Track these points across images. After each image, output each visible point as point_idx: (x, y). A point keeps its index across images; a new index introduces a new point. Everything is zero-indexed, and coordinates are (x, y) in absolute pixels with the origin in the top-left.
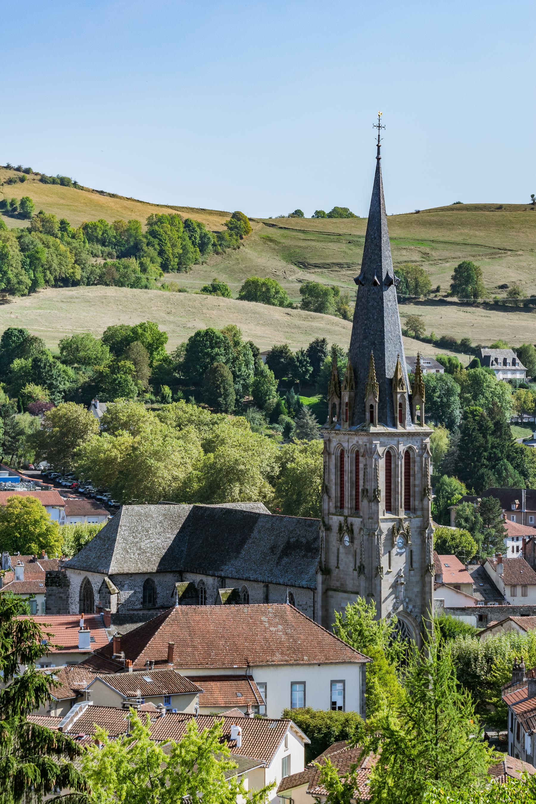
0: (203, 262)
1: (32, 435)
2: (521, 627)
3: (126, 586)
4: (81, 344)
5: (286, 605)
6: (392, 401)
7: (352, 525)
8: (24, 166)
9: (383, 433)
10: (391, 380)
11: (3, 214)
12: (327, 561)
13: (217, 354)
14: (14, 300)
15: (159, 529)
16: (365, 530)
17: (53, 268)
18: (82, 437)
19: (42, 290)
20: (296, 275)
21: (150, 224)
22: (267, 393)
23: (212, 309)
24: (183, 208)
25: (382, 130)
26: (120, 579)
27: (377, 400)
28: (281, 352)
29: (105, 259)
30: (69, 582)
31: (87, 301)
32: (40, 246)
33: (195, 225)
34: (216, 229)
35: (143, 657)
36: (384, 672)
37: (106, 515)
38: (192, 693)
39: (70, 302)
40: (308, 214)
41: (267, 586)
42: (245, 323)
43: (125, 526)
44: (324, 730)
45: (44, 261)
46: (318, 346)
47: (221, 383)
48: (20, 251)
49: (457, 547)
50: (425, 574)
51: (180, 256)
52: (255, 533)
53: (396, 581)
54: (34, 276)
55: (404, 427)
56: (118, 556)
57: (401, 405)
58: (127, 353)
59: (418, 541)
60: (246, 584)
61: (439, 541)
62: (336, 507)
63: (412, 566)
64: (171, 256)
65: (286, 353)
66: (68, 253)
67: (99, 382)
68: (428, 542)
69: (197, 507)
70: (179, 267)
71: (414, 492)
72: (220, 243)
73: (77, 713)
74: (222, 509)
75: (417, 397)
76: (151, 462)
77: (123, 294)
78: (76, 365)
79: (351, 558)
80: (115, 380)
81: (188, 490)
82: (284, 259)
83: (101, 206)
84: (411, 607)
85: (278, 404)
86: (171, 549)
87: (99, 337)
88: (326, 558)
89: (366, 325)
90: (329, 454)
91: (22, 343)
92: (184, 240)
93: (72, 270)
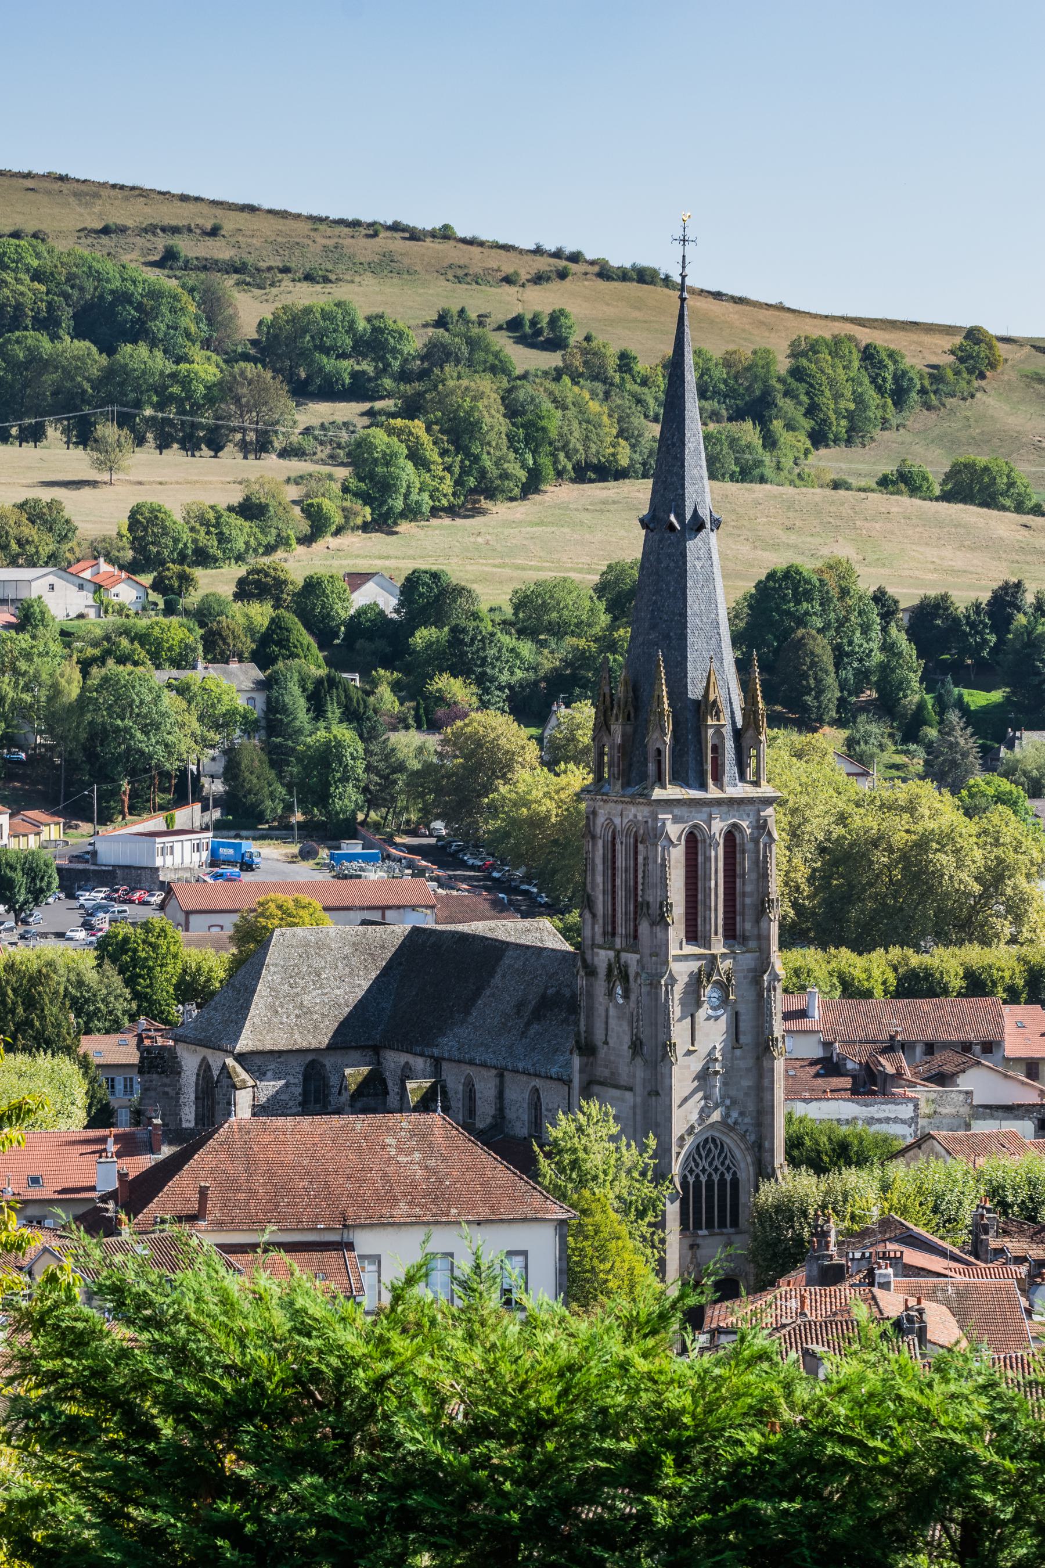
0: (898, 426)
3: (269, 1074)
4: (552, 597)
6: (700, 742)
7: (626, 966)
8: (569, 248)
9: (678, 801)
11: (516, 343)
13: (807, 613)
14: (494, 509)
16: (644, 975)
17: (571, 446)
18: (503, 776)
21: (793, 355)
22: (902, 685)
23: (874, 519)
24: (876, 320)
25: (689, 247)
26: (258, 1061)
27: (667, 739)
28: (937, 606)
30: (181, 1067)
32: (547, 405)
33: (884, 355)
34: (935, 360)
39: (601, 511)
41: (501, 1076)
42: (937, 546)
43: (276, 965)
45: (553, 434)
46: (1006, 594)
47: (810, 668)
48: (505, 416)
50: (764, 1055)
51: (850, 416)
52: (497, 980)
53: (706, 1069)
54: (535, 463)
55: (721, 788)
57: (715, 748)
59: (750, 995)
60: (470, 1070)
63: (737, 1040)
64: (833, 417)
65: (948, 608)
67: (580, 667)
68: (769, 997)
70: (850, 437)
71: (744, 905)
72: (934, 387)
75: (750, 733)
78: (542, 637)
83: (712, 322)
84: (735, 1114)
85: (921, 706)
86: (361, 1006)
88: (587, 1025)
89: (655, 602)
91: (437, 597)
92: (861, 384)
93: (612, 450)
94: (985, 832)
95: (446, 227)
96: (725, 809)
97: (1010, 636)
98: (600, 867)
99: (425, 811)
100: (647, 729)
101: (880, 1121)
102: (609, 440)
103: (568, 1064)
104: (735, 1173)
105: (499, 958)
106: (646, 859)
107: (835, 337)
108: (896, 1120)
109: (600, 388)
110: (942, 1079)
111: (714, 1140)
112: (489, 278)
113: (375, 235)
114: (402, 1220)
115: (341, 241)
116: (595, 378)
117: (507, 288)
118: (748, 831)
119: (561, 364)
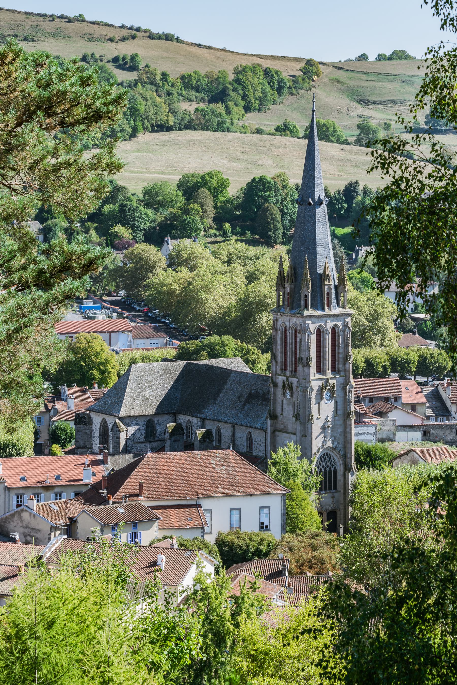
1: (114, 270)
2: (420, 457)
5: (229, 451)
6: (322, 291)
7: (292, 383)
8: (136, 26)
9: (314, 316)
10: (321, 275)
12: (275, 410)
13: (269, 196)
15: (159, 381)
16: (300, 387)
17: (150, 117)
18: (152, 272)
19: (142, 135)
20: (358, 111)
21: (236, 73)
24: (267, 56)
26: (128, 420)
27: (310, 291)
29: (199, 103)
31: (177, 144)
33: (273, 72)
34: (293, 73)
35: (120, 493)
36: (300, 499)
37: (165, 338)
38: (153, 519)
39: (163, 145)
40: (372, 58)
41: (234, 427)
43: (133, 379)
44: (244, 548)
45: (142, 112)
46: (351, 186)
49: (435, 363)
51: (260, 99)
52: (228, 385)
55: (331, 310)
56: (127, 403)
57: (328, 294)
58: (196, 198)
59: (342, 394)
60: (219, 424)
61: (421, 359)
62: (281, 370)
64: (253, 99)
66: (163, 104)
69: (189, 363)
71: (339, 358)
72: (294, 86)
73: (54, 544)
74: (206, 366)
75: (341, 287)
76: (203, 294)
77: (207, 137)
79: (291, 408)
80: (185, 220)
81: (227, 318)
82: (348, 97)
86: (168, 396)
87: (174, 185)
88: (273, 407)
89: (303, 234)
90: (276, 330)
92: (264, 85)
93: (166, 118)
94: (369, 299)
95: (80, 15)
96: (332, 318)
97: (354, 205)
98: (279, 342)
99: (118, 287)
100: (301, 287)
101: (361, 434)
102: (165, 114)
103: (265, 423)
104: (335, 467)
105: (229, 376)
106: (301, 340)
107: (252, 65)
108: (368, 434)
109: (154, 88)
110: (381, 414)
111: (327, 454)
112: (103, 39)
113: (53, 20)
114: (221, 495)
115: (39, 23)
116: (152, 84)
117: (110, 43)
118: (341, 327)
119: (137, 78)
